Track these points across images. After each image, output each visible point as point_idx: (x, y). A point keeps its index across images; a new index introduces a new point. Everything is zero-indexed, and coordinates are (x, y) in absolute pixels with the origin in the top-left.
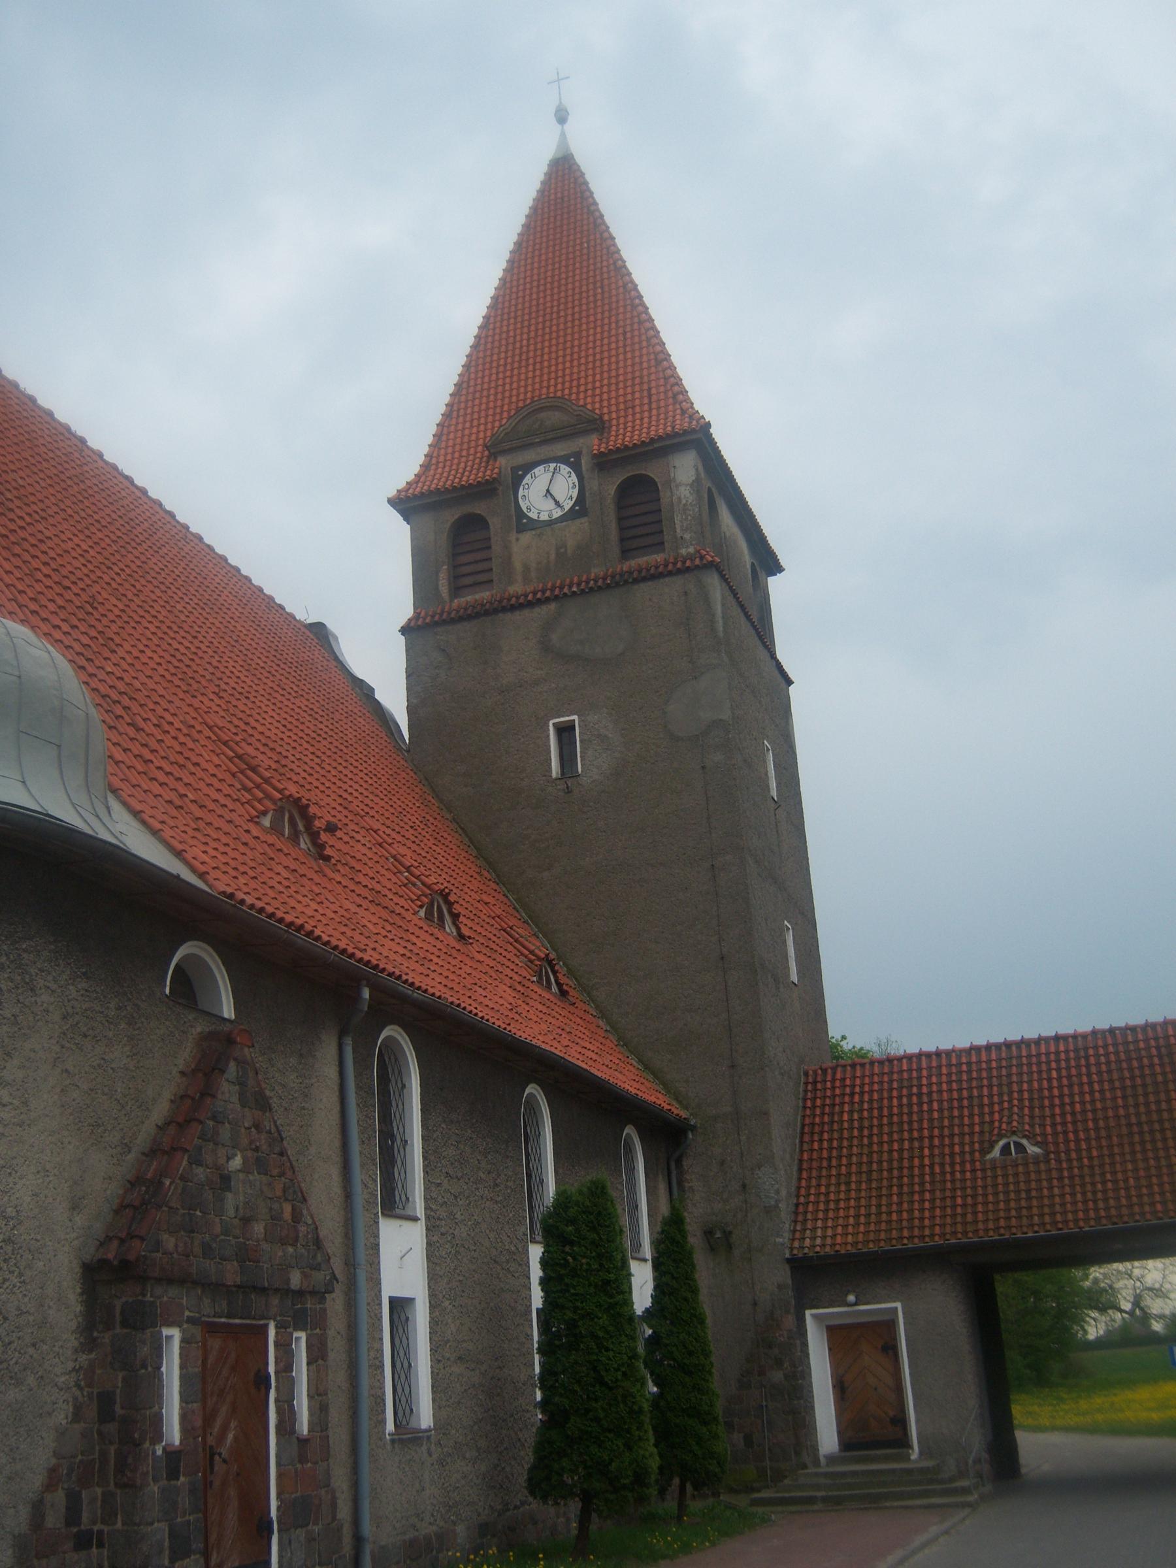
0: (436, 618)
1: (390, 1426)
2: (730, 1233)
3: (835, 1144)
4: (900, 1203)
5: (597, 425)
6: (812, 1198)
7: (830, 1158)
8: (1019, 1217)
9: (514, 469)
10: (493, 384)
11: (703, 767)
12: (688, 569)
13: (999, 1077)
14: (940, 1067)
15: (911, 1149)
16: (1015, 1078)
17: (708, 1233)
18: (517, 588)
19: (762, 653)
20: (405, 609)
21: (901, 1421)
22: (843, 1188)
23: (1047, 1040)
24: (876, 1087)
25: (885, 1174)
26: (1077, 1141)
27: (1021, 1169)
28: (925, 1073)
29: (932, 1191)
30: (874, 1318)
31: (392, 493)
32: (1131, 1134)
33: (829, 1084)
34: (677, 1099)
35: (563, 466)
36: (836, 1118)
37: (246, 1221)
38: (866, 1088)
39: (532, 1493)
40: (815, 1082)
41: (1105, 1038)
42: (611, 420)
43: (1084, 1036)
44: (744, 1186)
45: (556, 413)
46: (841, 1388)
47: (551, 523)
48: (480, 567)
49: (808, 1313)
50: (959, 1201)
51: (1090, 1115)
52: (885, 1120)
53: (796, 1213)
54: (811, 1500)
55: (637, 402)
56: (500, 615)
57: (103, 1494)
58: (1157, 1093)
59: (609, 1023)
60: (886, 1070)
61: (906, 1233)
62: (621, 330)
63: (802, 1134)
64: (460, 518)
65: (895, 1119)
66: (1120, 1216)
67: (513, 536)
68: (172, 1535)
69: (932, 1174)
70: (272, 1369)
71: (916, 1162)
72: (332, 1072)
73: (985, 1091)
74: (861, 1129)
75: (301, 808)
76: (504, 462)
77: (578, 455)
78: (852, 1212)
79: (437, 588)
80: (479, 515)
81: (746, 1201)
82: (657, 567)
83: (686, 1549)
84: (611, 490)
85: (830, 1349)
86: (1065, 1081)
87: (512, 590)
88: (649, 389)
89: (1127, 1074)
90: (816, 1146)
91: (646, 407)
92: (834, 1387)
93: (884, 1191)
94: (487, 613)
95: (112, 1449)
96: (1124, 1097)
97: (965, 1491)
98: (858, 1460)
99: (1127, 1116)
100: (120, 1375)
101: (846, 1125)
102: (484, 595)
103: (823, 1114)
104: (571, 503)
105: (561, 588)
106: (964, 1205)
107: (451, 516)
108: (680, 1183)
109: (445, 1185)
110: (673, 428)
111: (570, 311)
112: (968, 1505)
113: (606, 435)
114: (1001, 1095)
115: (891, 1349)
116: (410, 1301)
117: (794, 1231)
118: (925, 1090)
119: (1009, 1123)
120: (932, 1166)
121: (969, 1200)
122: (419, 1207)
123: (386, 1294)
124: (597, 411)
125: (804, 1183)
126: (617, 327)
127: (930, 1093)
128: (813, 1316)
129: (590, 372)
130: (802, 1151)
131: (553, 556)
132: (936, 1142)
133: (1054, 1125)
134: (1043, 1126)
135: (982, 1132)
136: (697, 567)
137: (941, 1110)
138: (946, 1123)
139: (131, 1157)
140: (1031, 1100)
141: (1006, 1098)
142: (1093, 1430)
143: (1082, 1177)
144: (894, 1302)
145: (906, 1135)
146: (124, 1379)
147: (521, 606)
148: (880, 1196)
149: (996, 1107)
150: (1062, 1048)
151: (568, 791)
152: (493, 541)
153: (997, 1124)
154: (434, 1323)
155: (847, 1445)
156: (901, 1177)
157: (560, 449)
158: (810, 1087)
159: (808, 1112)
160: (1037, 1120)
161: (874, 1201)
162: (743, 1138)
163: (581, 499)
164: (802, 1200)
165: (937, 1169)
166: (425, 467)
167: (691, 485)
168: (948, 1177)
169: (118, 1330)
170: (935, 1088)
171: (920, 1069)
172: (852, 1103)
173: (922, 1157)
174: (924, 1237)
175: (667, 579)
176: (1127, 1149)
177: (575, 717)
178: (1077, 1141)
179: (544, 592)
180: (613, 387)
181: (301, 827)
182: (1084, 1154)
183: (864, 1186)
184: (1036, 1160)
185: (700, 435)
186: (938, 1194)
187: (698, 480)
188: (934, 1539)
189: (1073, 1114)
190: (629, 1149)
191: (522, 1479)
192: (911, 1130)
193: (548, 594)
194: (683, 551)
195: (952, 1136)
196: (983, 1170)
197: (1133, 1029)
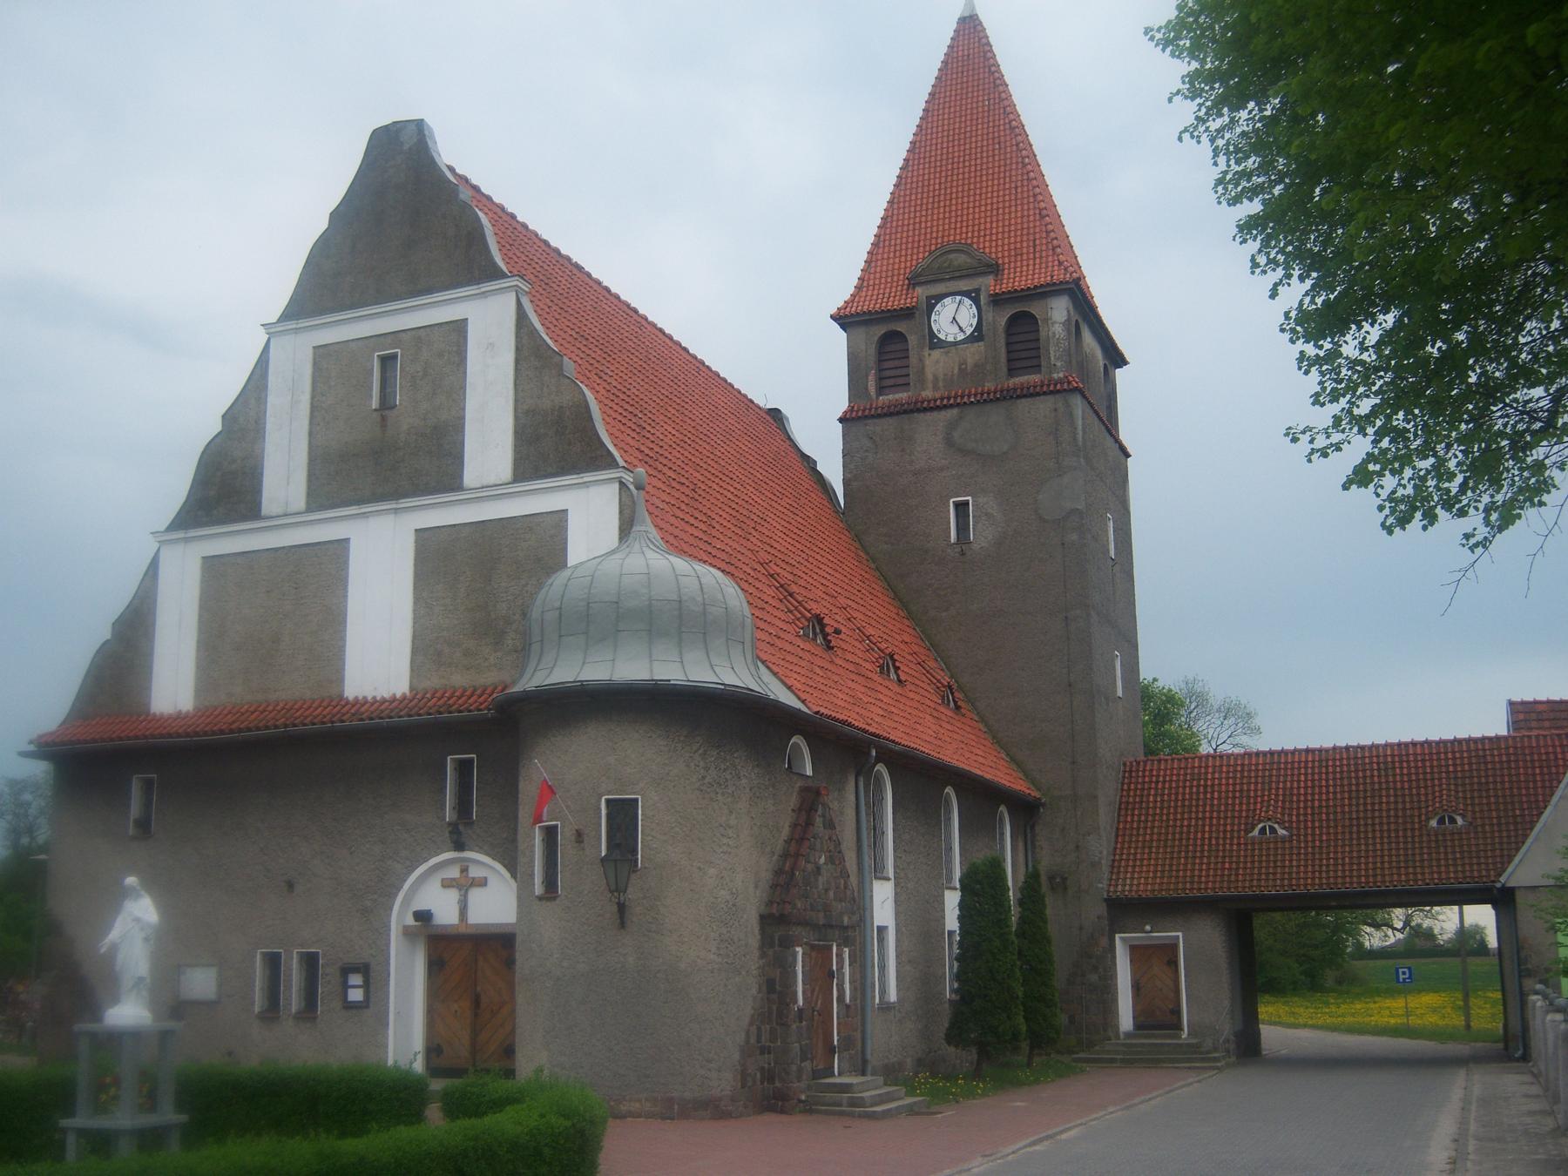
1: (877, 1001)
2: (1066, 878)
3: (1143, 818)
4: (1186, 864)
5: (994, 269)
6: (1124, 857)
7: (1138, 829)
8: (1267, 880)
9: (929, 298)
10: (912, 222)
11: (1063, 544)
12: (1058, 392)
13: (1263, 777)
14: (1221, 766)
15: (1196, 825)
16: (1274, 779)
17: (1051, 878)
18: (928, 393)
19: (1109, 441)
20: (842, 404)
21: (1177, 1012)
22: (1147, 851)
23: (1300, 751)
24: (1174, 778)
25: (1177, 843)
26: (1313, 828)
27: (1272, 846)
28: (1210, 770)
29: (1209, 857)
30: (522, 846)
31: (834, 310)
32: (1351, 826)
33: (1140, 774)
34: (1033, 784)
35: (966, 299)
36: (1145, 799)
37: (826, 890)
38: (1168, 779)
39: (949, 1043)
40: (1131, 771)
41: (1341, 753)
42: (1004, 264)
43: (1327, 750)
44: (1077, 847)
46: (1137, 988)
47: (955, 344)
48: (898, 372)
49: (1117, 936)
50: (1227, 866)
51: (1324, 810)
52: (1179, 803)
53: (1113, 867)
54: (1112, 1061)
55: (1025, 250)
58: (1373, 797)
59: (986, 725)
60: (1182, 766)
61: (1188, 886)
62: (1013, 185)
63: (1120, 809)
64: (885, 334)
65: (1187, 803)
66: (1336, 884)
68: (801, 1049)
69: (1210, 845)
70: (835, 968)
71: (1199, 835)
72: (852, 798)
73: (1252, 787)
74: (1162, 809)
75: (819, 619)
77: (977, 291)
78: (1152, 868)
79: (867, 389)
81: (1078, 857)
82: (1035, 387)
83: (1037, 1082)
85: (1131, 961)
86: (1309, 784)
87: (924, 394)
89: (1354, 781)
90: (1129, 819)
91: (1031, 256)
92: (1132, 986)
93: (1175, 855)
94: (905, 412)
95: (774, 1007)
96: (1350, 798)
97: (1216, 1060)
98: (1146, 1037)
99: (1350, 812)
101: (1151, 805)
102: (902, 396)
103: (1135, 795)
105: (962, 397)
106: (1230, 869)
107: (880, 330)
108: (1033, 842)
109: (904, 858)
111: (973, 163)
112: (1218, 1068)
113: (1000, 277)
114: (1263, 790)
115: (1173, 963)
116: (886, 927)
117: (1111, 879)
118: (1209, 783)
119: (1267, 812)
120: (1210, 839)
121: (1234, 866)
122: (891, 873)
123: (876, 923)
125: (1119, 846)
127: (1213, 785)
128: (1121, 938)
130: (1119, 822)
131: (956, 371)
132: (1215, 821)
133: (1298, 815)
134: (1290, 815)
135: (1247, 817)
137: (1220, 798)
138: (1223, 808)
139: (775, 857)
140: (1284, 795)
141: (1266, 793)
142: (1351, 1030)
143: (1313, 854)
145: (1193, 815)
147: (931, 409)
148: (1172, 858)
149: (1259, 799)
150: (1310, 759)
151: (963, 553)
152: (911, 353)
153: (1258, 812)
154: (898, 941)
155: (1139, 1026)
156: (1187, 846)
157: (964, 285)
158: (1127, 775)
159: (1125, 793)
160: (1287, 811)
161: (1168, 862)
162: (1079, 813)
164: (1117, 857)
165: (1214, 842)
167: (1064, 324)
168: (1221, 848)
169: (776, 948)
170: (1216, 782)
171: (1207, 767)
172: (1156, 789)
173: (1203, 832)
174: (1200, 889)
175: (1042, 397)
176: (1347, 837)
177: (969, 498)
178: (1313, 828)
179: (949, 398)
180: (1006, 235)
181: (818, 630)
182: (1317, 838)
183: (1161, 850)
184: (1283, 841)
185: (1072, 286)
186: (1213, 860)
187: (1068, 320)
188: (1191, 1084)
189: (1313, 808)
190: (1002, 820)
191: (942, 1035)
192: (1197, 812)
193: (952, 401)
194: (1055, 376)
195: (1226, 818)
196: (1246, 844)
197: (1362, 748)
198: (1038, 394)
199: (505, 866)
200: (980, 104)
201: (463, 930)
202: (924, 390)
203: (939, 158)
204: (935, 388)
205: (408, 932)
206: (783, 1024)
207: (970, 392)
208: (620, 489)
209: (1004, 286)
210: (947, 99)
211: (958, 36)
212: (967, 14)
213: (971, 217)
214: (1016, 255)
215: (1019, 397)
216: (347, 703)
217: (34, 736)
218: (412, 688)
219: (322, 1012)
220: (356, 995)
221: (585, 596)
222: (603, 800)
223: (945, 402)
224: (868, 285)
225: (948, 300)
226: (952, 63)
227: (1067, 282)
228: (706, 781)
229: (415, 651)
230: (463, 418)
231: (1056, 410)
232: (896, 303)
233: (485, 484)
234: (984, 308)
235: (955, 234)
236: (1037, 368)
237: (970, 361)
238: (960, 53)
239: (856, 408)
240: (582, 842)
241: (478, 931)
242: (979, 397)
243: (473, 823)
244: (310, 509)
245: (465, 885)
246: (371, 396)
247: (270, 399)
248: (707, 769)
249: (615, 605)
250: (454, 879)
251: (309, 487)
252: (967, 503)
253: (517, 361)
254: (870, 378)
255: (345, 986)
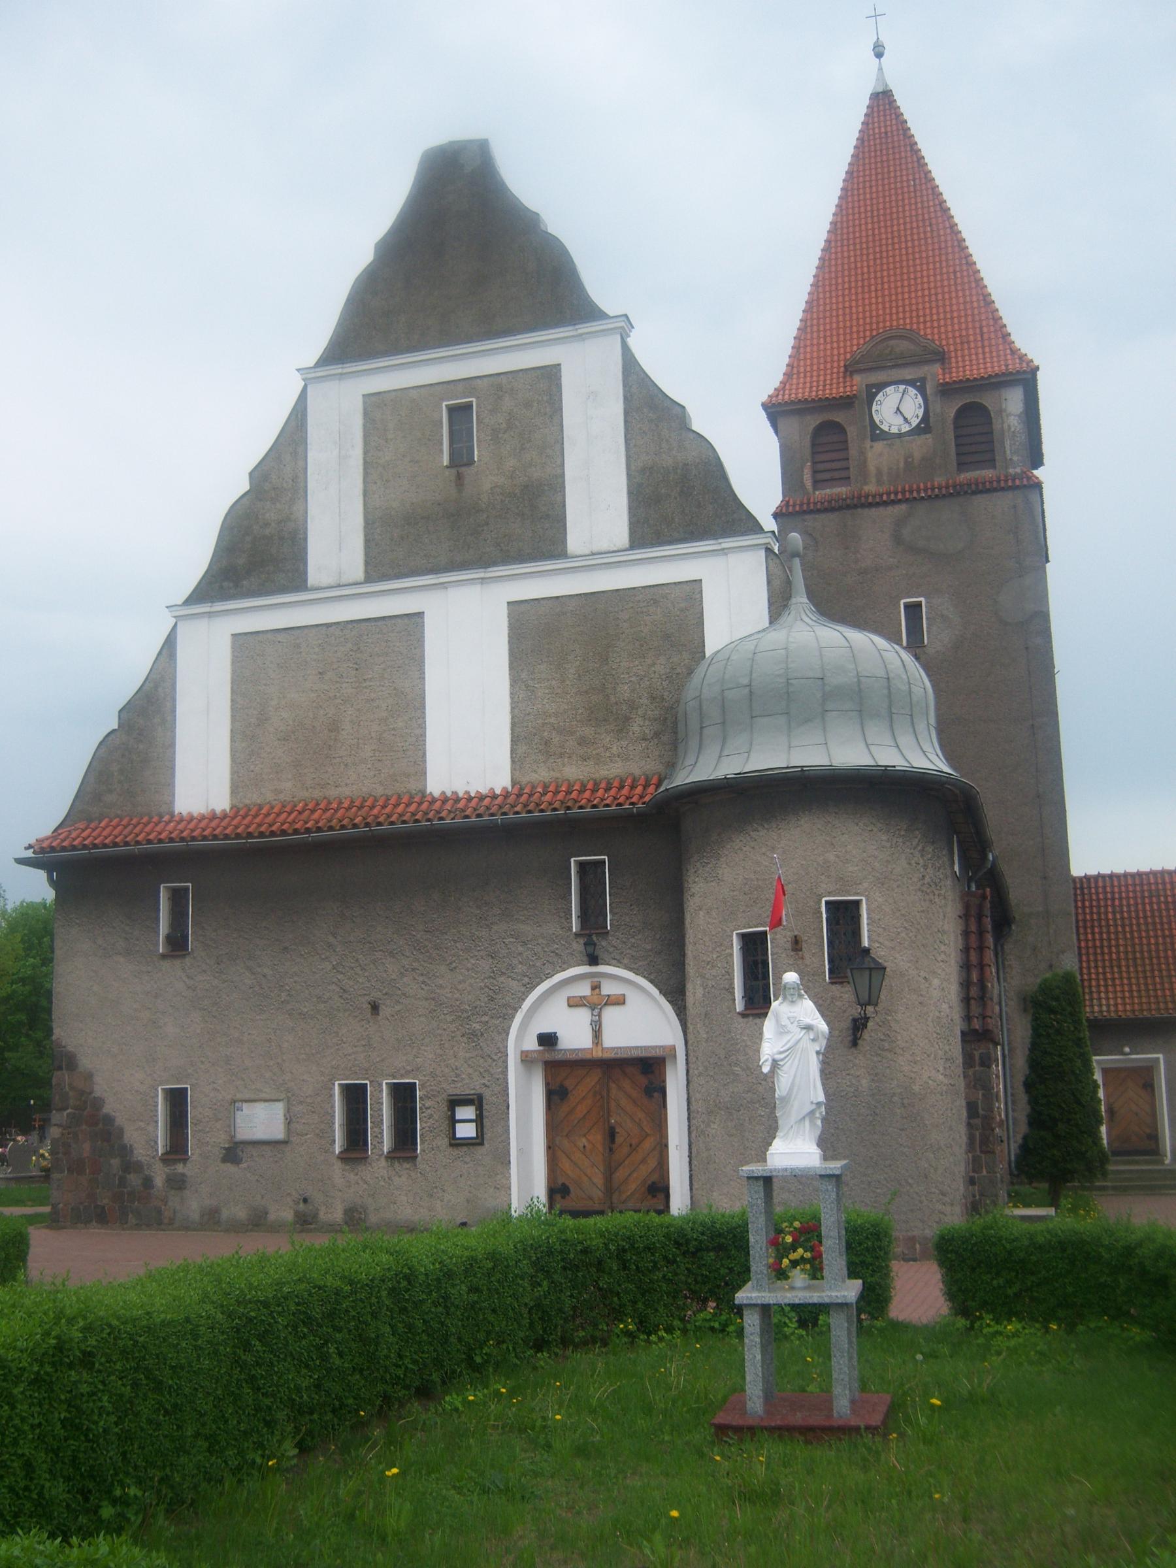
0: (797, 508)
5: (940, 357)
11: (1027, 648)
12: (1018, 487)
18: (871, 488)
30: (1140, 1064)
35: (910, 389)
45: (905, 342)
47: (900, 436)
56: (859, 510)
57: (973, 1157)
67: (868, 443)
76: (859, 381)
77: (923, 380)
79: (802, 482)
80: (838, 423)
84: (951, 412)
87: (866, 488)
88: (981, 328)
91: (980, 344)
94: (848, 507)
100: (981, 1093)
102: (842, 490)
104: (918, 421)
105: (911, 492)
107: (813, 421)
110: (1007, 366)
124: (937, 342)
126: (948, 266)
129: (927, 305)
131: (902, 465)
136: (1025, 486)
144: (1157, 1053)
146: (983, 1095)
147: (877, 504)
152: (850, 445)
154: (1139, 1059)
157: (909, 373)
162: (1051, 931)
163: (926, 418)
166: (788, 375)
167: (1019, 416)
169: (977, 1068)
177: (922, 599)
179: (896, 494)
193: (900, 496)
194: (1011, 471)
198: (995, 490)
199: (651, 981)
200: (905, 184)
201: (598, 1054)
202: (866, 484)
203: (864, 240)
204: (879, 482)
205: (526, 1059)
206: (989, 1152)
207: (918, 487)
208: (766, 557)
209: (954, 375)
210: (867, 178)
211: (873, 112)
212: (880, 90)
213: (907, 302)
214: (962, 343)
215: (974, 493)
216: (181, 820)
217: (32, 841)
218: (514, 783)
219: (423, 1151)
220: (466, 1131)
221: (782, 671)
222: (823, 903)
223: (892, 497)
224: (799, 373)
225: (890, 390)
226: (869, 140)
227: (1025, 372)
228: (927, 880)
229: (515, 740)
230: (563, 475)
231: (1015, 507)
232: (835, 390)
233: (595, 550)
234: (930, 398)
235: (891, 320)
236: (991, 463)
237: (917, 455)
238: (877, 131)
239: (791, 503)
240: (801, 950)
241: (619, 1056)
242: (929, 492)
243: (189, 953)
244: (369, 579)
245: (597, 1003)
246: (441, 451)
247: (311, 456)
248: (925, 867)
249: (820, 682)
250: (584, 997)
251: (367, 554)
252: (919, 605)
253: (627, 413)
254: (806, 471)
255: (453, 1121)
